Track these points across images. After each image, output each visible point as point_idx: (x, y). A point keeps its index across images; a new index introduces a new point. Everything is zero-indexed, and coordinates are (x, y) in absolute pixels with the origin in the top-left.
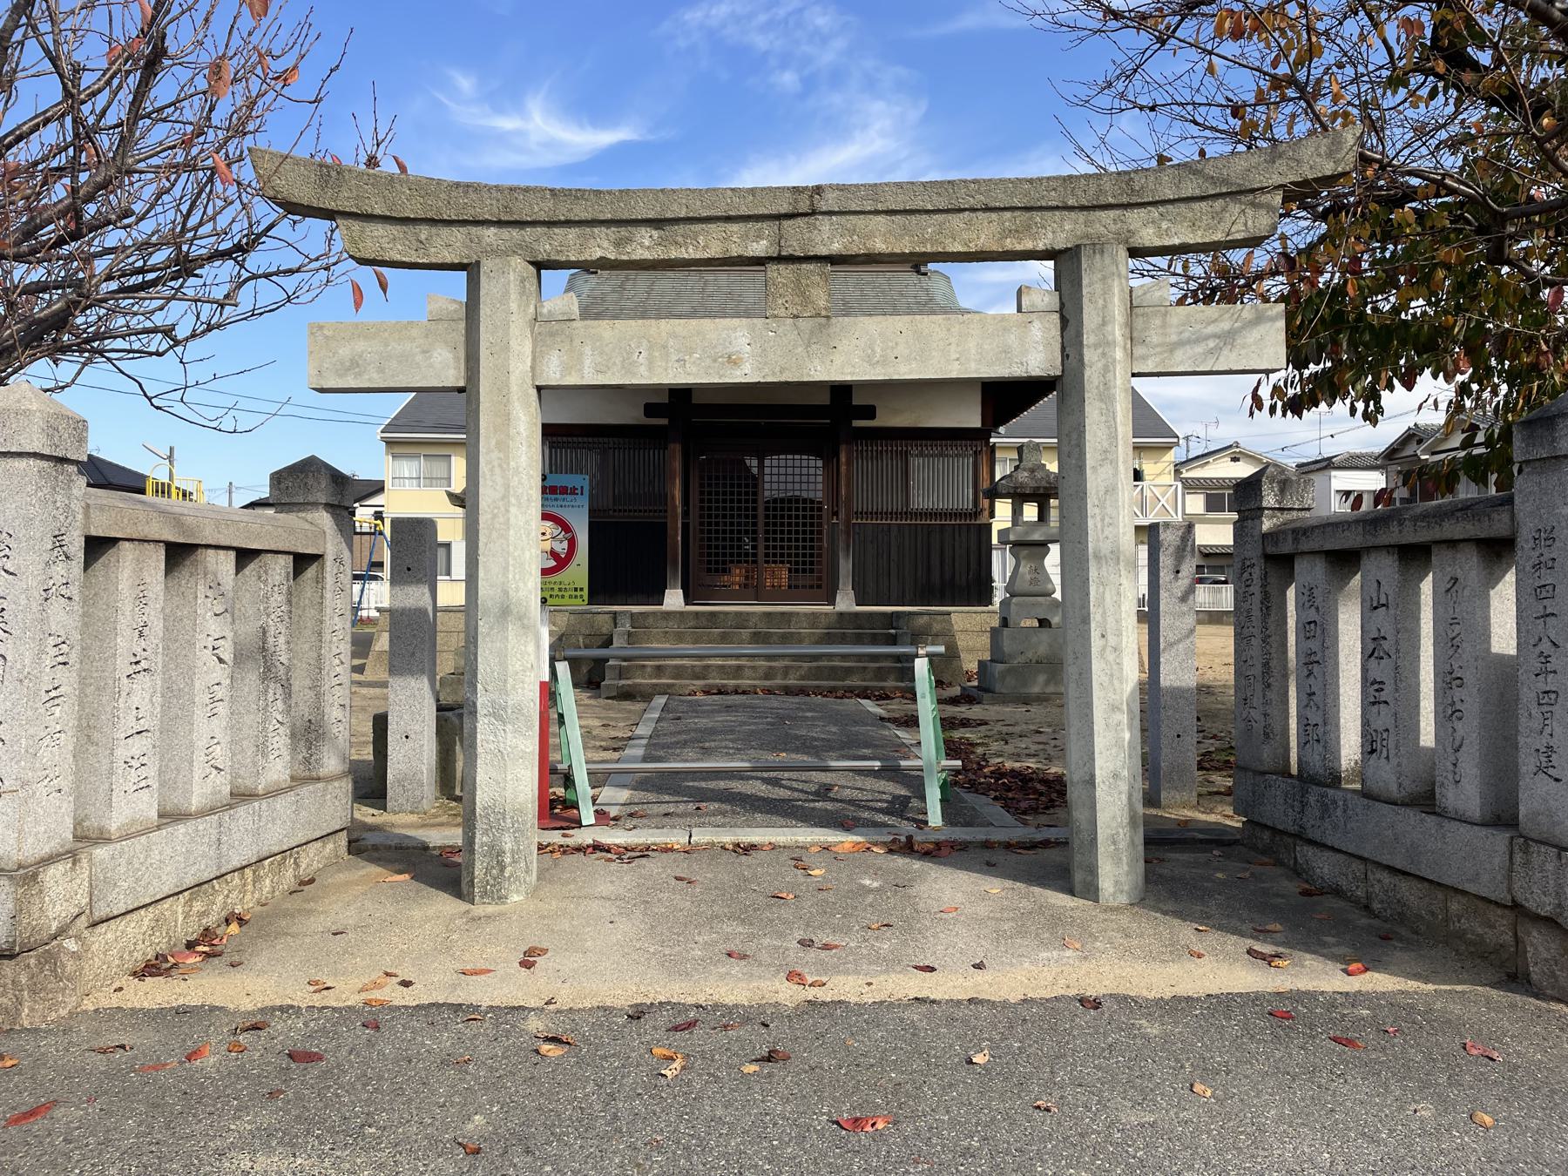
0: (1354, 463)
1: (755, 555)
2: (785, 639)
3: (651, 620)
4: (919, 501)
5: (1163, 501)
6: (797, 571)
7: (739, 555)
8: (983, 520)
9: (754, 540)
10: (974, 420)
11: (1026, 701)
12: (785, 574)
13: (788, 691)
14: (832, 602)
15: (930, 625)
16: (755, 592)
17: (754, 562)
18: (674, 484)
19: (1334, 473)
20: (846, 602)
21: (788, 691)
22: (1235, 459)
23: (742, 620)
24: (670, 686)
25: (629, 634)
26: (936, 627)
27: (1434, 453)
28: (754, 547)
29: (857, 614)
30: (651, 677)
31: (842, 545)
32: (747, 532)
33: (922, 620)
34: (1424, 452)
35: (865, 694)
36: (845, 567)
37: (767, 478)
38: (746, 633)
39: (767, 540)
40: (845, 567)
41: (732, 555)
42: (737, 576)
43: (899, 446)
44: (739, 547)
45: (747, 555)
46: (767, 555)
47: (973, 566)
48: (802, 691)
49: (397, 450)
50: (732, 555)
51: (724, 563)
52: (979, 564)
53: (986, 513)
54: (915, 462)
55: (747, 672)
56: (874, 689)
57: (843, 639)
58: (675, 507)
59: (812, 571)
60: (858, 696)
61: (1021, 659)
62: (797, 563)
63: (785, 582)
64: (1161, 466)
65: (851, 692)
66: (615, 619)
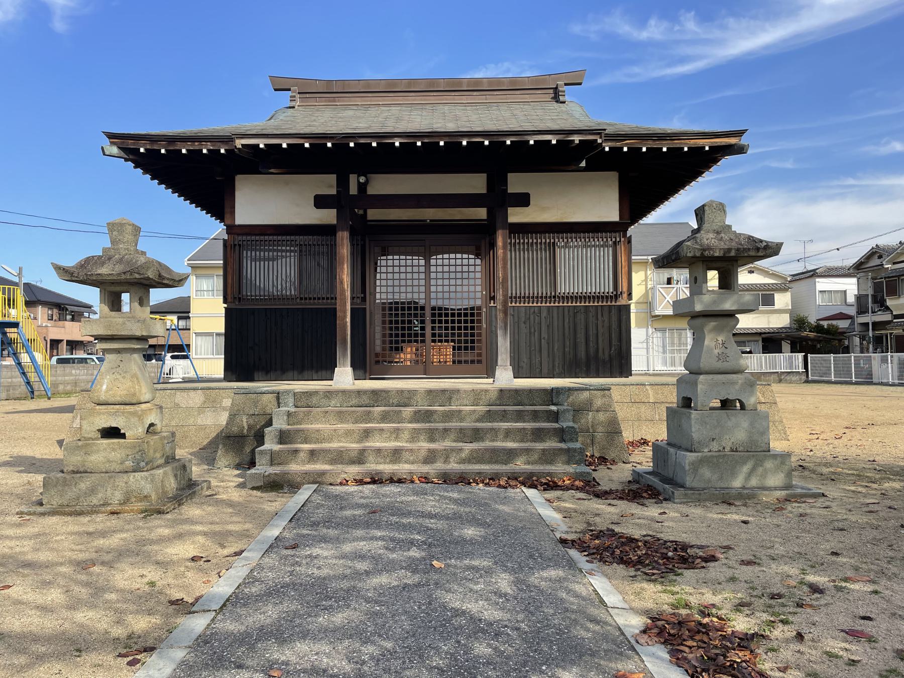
0: (831, 273)
1: (423, 335)
3: (314, 400)
4: (563, 288)
6: (460, 348)
7: (410, 335)
8: (622, 301)
9: (423, 322)
10: (610, 212)
11: (727, 500)
12: (450, 351)
13: (447, 479)
14: (490, 373)
16: (424, 368)
17: (423, 341)
18: (343, 268)
19: (817, 280)
20: (504, 377)
21: (447, 479)
22: (751, 272)
23: (406, 398)
24: (323, 473)
25: (289, 414)
26: (598, 402)
27: (894, 263)
28: (423, 329)
29: (517, 392)
30: (303, 463)
31: (500, 324)
32: (416, 315)
34: (888, 263)
35: (530, 481)
36: (504, 345)
38: (408, 411)
39: (433, 322)
40: (504, 345)
41: (403, 335)
42: (407, 355)
43: (548, 238)
44: (410, 329)
45: (416, 335)
46: (434, 335)
47: (615, 342)
48: (463, 479)
49: (199, 272)
50: (403, 335)
51: (397, 342)
52: (620, 340)
53: (625, 295)
54: (561, 254)
55: (406, 455)
56: (540, 475)
57: (503, 416)
58: (343, 290)
59: (473, 348)
60: (523, 484)
61: (715, 446)
62: (460, 342)
63: (450, 358)
65: (516, 479)
66: (278, 398)
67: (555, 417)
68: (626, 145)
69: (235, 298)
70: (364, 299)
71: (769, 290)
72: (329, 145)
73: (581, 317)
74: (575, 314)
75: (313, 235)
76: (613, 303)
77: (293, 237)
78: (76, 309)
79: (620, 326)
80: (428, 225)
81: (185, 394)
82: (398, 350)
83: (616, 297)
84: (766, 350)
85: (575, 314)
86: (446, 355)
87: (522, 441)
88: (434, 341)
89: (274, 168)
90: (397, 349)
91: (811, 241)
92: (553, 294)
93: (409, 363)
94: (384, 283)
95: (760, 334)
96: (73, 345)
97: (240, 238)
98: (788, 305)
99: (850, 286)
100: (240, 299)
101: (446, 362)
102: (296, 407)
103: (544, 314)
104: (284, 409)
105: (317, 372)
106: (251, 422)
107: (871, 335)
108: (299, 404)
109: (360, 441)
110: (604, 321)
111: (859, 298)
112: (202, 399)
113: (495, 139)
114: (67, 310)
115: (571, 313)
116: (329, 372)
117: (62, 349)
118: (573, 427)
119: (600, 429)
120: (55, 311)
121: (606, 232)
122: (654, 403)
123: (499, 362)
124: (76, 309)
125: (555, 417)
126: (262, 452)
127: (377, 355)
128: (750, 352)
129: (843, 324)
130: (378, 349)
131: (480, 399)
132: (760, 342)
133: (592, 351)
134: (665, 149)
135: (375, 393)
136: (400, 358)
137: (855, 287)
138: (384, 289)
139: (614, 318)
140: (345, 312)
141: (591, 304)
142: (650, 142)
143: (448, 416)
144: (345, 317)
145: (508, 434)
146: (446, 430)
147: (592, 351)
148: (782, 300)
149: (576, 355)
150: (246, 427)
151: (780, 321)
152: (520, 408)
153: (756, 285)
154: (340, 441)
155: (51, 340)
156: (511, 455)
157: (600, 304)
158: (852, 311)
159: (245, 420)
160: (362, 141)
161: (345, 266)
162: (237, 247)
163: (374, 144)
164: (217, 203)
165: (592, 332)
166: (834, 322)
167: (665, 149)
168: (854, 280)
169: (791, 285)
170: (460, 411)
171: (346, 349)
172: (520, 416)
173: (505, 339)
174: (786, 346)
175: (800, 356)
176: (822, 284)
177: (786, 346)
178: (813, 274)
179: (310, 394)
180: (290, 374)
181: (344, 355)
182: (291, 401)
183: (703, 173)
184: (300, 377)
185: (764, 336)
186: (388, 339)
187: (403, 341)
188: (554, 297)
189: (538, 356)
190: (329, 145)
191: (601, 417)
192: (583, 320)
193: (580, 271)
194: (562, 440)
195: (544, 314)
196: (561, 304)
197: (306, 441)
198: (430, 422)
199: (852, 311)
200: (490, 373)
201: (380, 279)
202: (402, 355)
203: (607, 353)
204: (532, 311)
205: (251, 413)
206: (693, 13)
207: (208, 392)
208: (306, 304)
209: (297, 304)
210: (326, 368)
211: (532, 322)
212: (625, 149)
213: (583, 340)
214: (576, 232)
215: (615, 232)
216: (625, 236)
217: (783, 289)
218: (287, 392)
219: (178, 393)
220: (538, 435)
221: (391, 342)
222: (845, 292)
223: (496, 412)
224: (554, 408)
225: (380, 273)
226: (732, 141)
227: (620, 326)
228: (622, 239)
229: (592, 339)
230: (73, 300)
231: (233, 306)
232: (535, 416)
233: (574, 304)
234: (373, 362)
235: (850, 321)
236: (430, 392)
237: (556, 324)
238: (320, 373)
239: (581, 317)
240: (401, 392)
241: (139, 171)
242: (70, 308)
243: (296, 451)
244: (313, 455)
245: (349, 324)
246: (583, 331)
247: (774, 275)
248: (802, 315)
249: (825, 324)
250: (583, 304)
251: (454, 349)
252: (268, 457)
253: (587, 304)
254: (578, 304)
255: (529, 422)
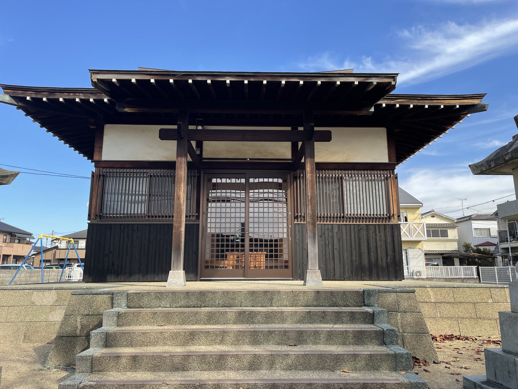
1: (243, 246)
2: (269, 317)
3: (145, 300)
4: (349, 210)
5: (418, 230)
7: (232, 246)
8: (394, 221)
10: (383, 157)
12: (263, 258)
14: (302, 277)
15: (398, 303)
17: (243, 251)
18: (180, 186)
19: (472, 222)
22: (433, 217)
23: (229, 299)
25: (119, 315)
30: (125, 369)
31: (309, 234)
33: (391, 298)
37: (251, 225)
41: (227, 246)
45: (237, 246)
47: (390, 253)
50: (227, 246)
51: (222, 251)
52: (394, 251)
53: (396, 217)
55: (231, 362)
57: (323, 317)
58: (180, 205)
63: (263, 264)
64: (415, 215)
66: (112, 299)
67: (371, 318)
68: (398, 102)
69: (97, 216)
70: (198, 217)
71: (444, 227)
72: (171, 81)
73: (364, 233)
74: (359, 230)
75: (161, 169)
76: (387, 223)
77: (145, 171)
78: (21, 235)
79: (393, 241)
80: (248, 163)
81: (40, 294)
82: (224, 257)
83: (390, 218)
84: (445, 264)
85: (359, 230)
86: (261, 261)
87: (344, 344)
88: (251, 250)
89: (128, 107)
90: (222, 256)
91: (466, 199)
92: (342, 215)
93: (231, 268)
94: (213, 220)
95: (442, 254)
96: (17, 258)
97: (104, 170)
98: (455, 237)
99: (493, 226)
100: (100, 216)
101: (260, 267)
102: (129, 307)
103: (336, 230)
104: (116, 309)
105: (158, 275)
106: (85, 322)
107: (511, 255)
108: (132, 304)
109: (184, 344)
110: (381, 236)
111: (500, 232)
112: (55, 298)
113: (309, 80)
114: (16, 236)
115: (356, 230)
116: (164, 276)
117: (10, 261)
118: (393, 330)
119: (409, 329)
120: (8, 237)
121: (380, 170)
122: (435, 303)
123: (310, 267)
124: (21, 235)
125: (371, 318)
126: (82, 358)
127: (207, 262)
128: (437, 265)
129: (492, 249)
130: (208, 257)
131: (299, 300)
132: (441, 259)
133: (373, 259)
134: (427, 107)
135: (202, 294)
136: (224, 264)
137: (496, 226)
138: (213, 225)
139: (389, 234)
140: (180, 223)
141: (371, 223)
142: (416, 101)
143: (269, 317)
144: (180, 227)
145: (331, 337)
146: (270, 332)
147: (373, 259)
148: (452, 234)
149: (361, 262)
150: (79, 327)
151: (451, 247)
152: (335, 309)
153: (436, 224)
154: (165, 344)
155: (3, 255)
156: (334, 362)
157: (377, 223)
158: (496, 241)
159: (79, 320)
160: (199, 79)
161: (182, 185)
162: (101, 178)
163: (209, 81)
164: (86, 142)
165: (372, 244)
166: (487, 247)
167: (427, 107)
168: (496, 222)
169: (457, 225)
170: (282, 313)
171: (179, 254)
172: (338, 318)
173: (314, 246)
174: (457, 261)
175: (474, 268)
176: (476, 224)
177: (457, 261)
178: (470, 218)
179: (140, 295)
180: (137, 277)
181: (178, 259)
182: (124, 302)
183: (415, 152)
184: (156, 279)
185: (445, 255)
186: (215, 243)
187: (227, 251)
188: (343, 217)
189: (332, 263)
190: (171, 81)
191: (409, 318)
192: (365, 235)
193: (361, 199)
194: (383, 343)
195: (336, 230)
196: (348, 223)
197: (131, 345)
198: (253, 323)
199: (496, 241)
200: (302, 277)
201: (211, 213)
202: (226, 262)
203: (384, 261)
204: (326, 228)
205: (86, 313)
206: (370, 58)
207: (60, 292)
208: (153, 221)
209: (146, 221)
210: (161, 271)
211: (327, 236)
212: (398, 106)
213: (366, 251)
214: (357, 170)
215: (386, 170)
216: (393, 173)
217: (453, 227)
218: (121, 293)
219: (35, 292)
220: (360, 338)
221: (218, 246)
222: (489, 229)
223: (316, 313)
224: (369, 310)
225: (211, 213)
226: (476, 102)
227: (393, 241)
228: (392, 176)
229: (373, 249)
230: (20, 230)
231: (95, 222)
232: (353, 317)
233: (358, 223)
234: (203, 267)
235: (495, 247)
236: (253, 293)
237: (344, 238)
238: (160, 276)
239: (364, 233)
240: (226, 293)
241: (44, 129)
242: (17, 235)
243: (118, 357)
244: (135, 361)
245: (183, 233)
246: (366, 244)
247: (447, 219)
248: (467, 243)
249: (482, 248)
250: (364, 223)
251: (266, 256)
252: (89, 364)
253: (368, 223)
254: (361, 223)
255: (347, 323)
